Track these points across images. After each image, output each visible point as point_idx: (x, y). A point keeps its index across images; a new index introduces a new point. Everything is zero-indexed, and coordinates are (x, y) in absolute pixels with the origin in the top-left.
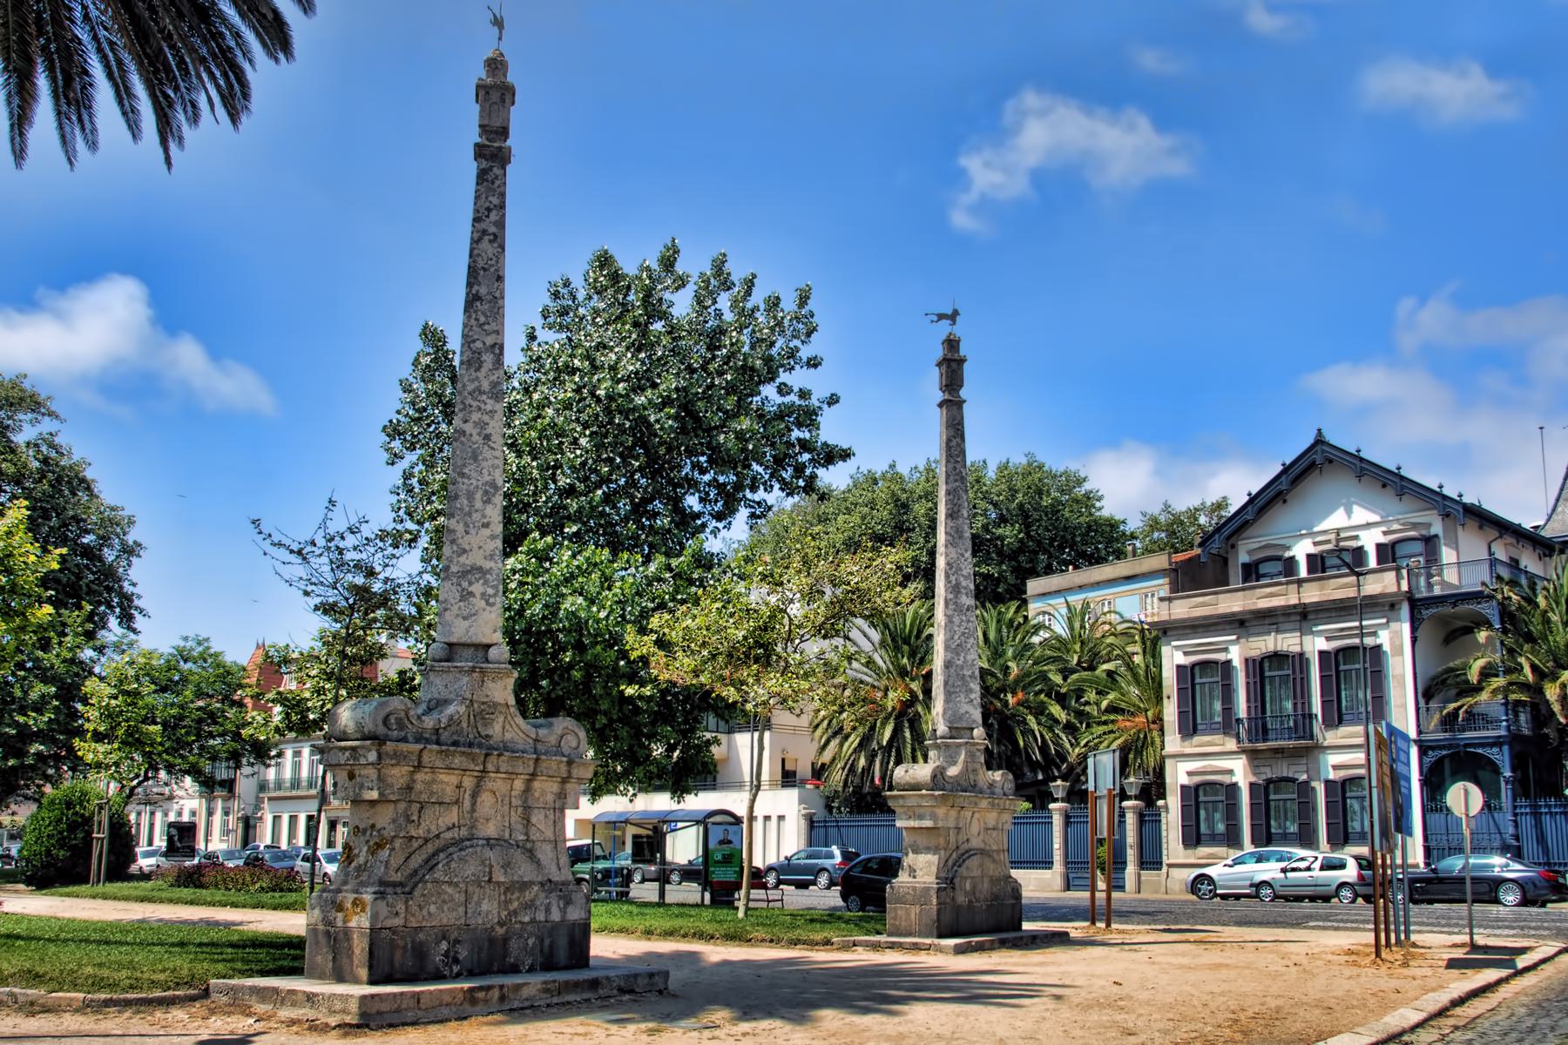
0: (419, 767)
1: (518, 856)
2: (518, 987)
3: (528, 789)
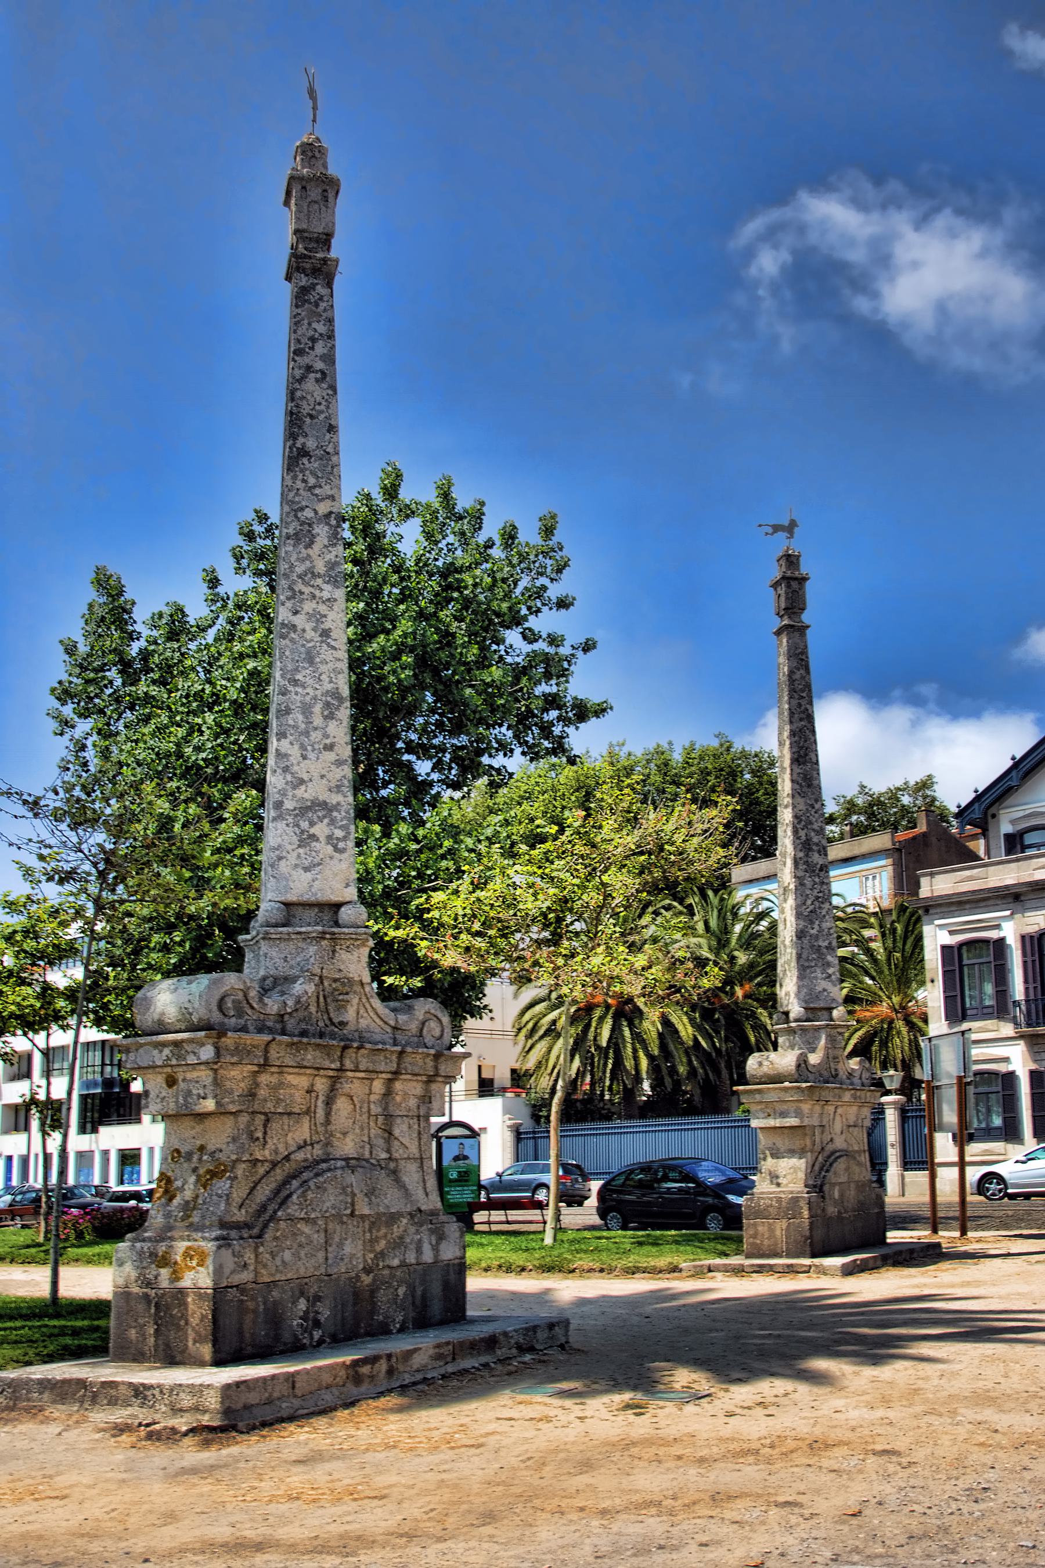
0: (265, 1065)
1: (384, 1181)
2: (408, 1354)
3: (388, 1093)
